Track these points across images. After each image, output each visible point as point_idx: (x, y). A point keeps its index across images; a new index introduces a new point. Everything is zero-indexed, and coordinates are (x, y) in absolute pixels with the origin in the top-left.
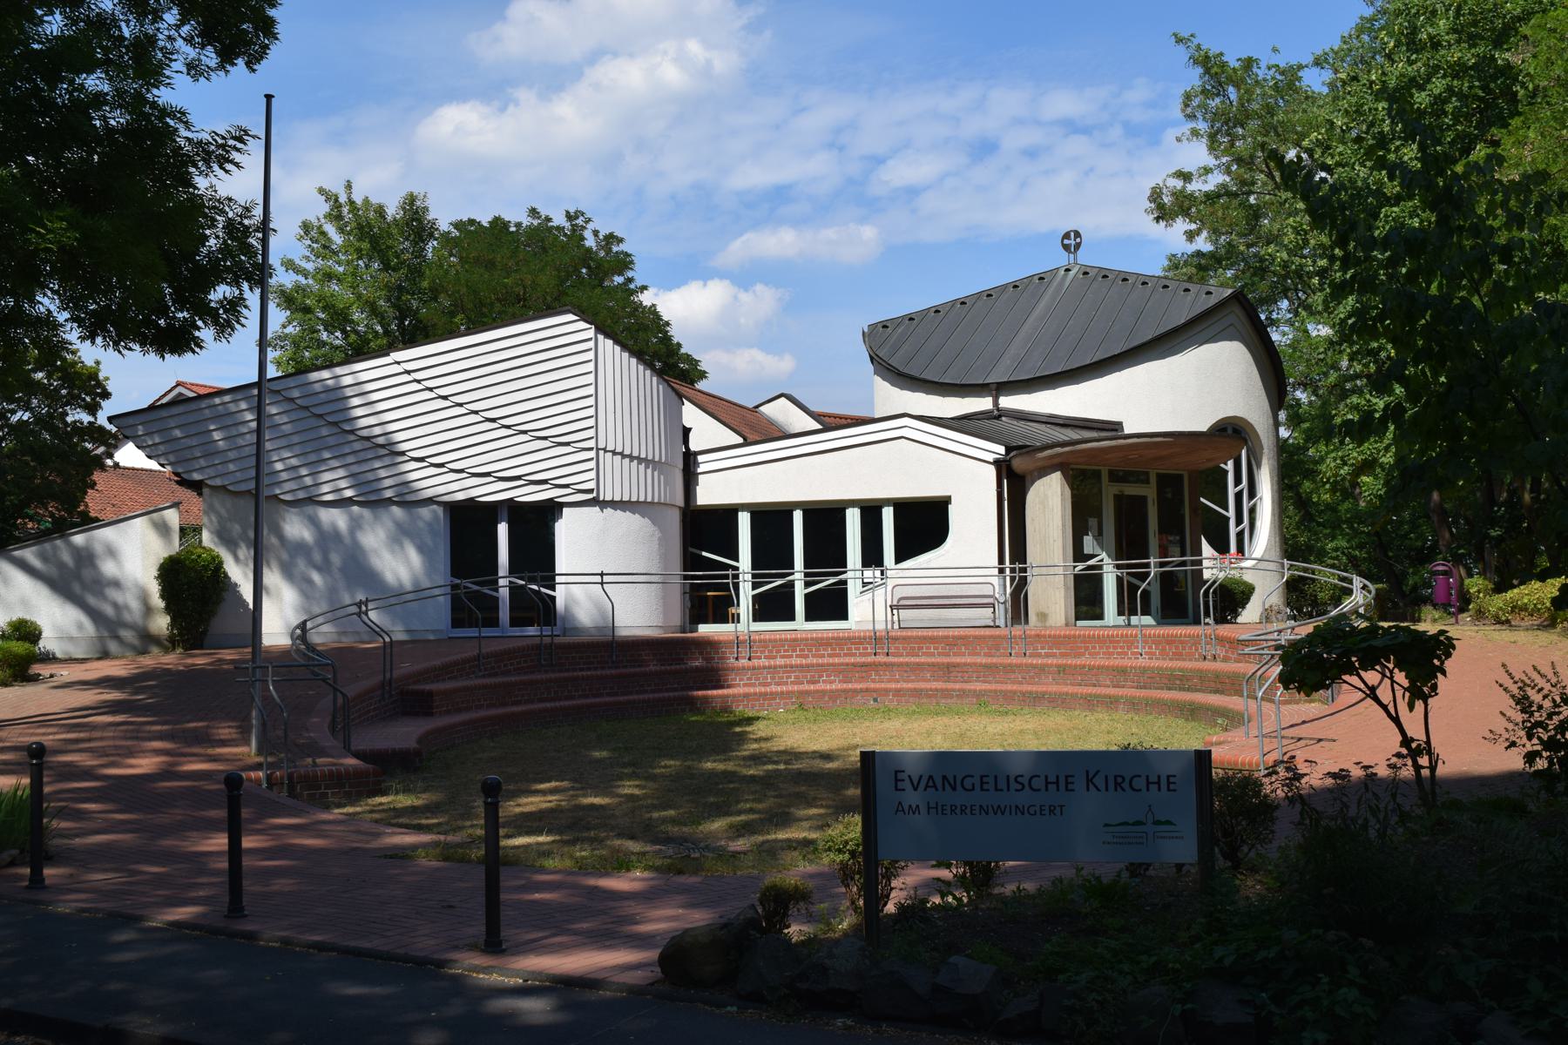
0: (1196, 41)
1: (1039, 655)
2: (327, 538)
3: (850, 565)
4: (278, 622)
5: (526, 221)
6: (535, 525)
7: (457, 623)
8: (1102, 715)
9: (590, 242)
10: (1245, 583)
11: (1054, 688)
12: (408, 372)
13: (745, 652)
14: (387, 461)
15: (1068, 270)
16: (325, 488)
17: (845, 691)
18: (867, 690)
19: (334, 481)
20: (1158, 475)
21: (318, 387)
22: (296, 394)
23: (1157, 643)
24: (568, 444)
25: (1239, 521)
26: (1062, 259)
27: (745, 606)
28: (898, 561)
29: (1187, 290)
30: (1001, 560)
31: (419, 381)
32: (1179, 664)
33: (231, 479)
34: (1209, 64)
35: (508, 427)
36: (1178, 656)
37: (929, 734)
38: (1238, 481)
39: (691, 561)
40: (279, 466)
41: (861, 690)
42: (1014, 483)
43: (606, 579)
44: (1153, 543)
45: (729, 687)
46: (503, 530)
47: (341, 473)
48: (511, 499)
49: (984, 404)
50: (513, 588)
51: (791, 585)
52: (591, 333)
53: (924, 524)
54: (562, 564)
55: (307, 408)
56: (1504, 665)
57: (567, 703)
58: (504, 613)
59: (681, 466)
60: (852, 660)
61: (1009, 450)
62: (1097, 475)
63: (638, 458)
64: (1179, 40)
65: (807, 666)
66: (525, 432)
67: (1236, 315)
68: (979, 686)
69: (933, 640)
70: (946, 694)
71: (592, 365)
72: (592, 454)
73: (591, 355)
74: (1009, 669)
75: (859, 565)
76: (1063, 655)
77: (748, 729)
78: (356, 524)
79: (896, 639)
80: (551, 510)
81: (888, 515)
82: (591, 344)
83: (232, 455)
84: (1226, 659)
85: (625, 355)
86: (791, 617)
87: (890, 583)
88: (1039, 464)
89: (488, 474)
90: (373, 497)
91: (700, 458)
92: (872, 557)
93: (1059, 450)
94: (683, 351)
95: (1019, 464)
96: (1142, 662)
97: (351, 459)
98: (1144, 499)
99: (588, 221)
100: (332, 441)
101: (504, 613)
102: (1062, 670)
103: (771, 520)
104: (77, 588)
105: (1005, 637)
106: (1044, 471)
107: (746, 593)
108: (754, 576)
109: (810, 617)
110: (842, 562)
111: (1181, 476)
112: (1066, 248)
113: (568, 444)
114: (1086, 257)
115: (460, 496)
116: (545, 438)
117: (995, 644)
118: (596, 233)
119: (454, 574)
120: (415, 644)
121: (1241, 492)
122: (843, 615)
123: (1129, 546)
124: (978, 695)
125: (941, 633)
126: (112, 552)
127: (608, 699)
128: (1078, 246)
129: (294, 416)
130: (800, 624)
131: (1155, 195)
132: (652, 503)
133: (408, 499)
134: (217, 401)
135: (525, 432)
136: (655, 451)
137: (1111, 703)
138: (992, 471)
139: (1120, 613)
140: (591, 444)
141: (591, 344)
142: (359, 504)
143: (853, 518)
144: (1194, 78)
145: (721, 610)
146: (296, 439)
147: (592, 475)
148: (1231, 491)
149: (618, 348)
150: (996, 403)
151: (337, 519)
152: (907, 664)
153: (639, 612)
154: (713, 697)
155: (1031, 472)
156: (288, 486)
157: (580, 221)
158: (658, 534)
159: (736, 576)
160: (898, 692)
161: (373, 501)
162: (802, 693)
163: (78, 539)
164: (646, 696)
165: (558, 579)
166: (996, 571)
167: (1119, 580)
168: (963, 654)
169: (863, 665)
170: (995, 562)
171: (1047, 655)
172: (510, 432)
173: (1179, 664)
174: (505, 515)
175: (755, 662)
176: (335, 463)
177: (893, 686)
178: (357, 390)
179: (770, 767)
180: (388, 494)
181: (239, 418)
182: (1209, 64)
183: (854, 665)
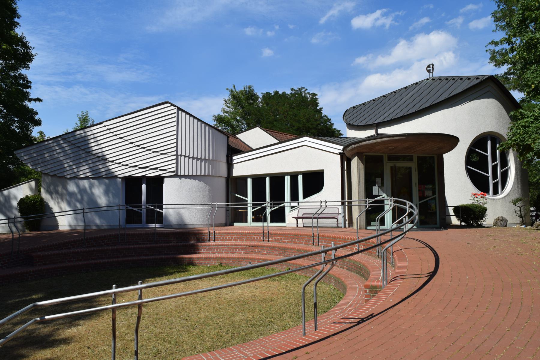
2: (82, 191)
3: (286, 200)
4: (65, 223)
6: (156, 184)
14: (102, 162)
16: (81, 173)
18: (247, 258)
19: (85, 171)
20: (418, 157)
21: (78, 136)
22: (71, 139)
24: (166, 154)
26: (427, 75)
28: (304, 198)
30: (343, 197)
35: (144, 148)
40: (66, 165)
45: (199, 253)
46: (144, 187)
47: (86, 167)
48: (145, 175)
50: (148, 210)
53: (314, 181)
54: (166, 200)
65: (231, 245)
66: (150, 150)
71: (176, 123)
72: (175, 157)
78: (91, 186)
81: (300, 178)
83: (51, 162)
89: (136, 166)
90: (97, 176)
92: (294, 197)
93: (353, 146)
95: (347, 154)
97: (90, 162)
98: (410, 168)
99: (306, 90)
103: (259, 180)
107: (250, 211)
110: (283, 199)
112: (429, 71)
113: (166, 154)
114: (437, 73)
115: (128, 174)
116: (157, 152)
122: (284, 221)
127: (144, 258)
133: (111, 177)
134: (46, 143)
135: (150, 150)
143: (287, 179)
146: (72, 155)
147: (175, 165)
150: (376, 132)
151: (85, 184)
153: (194, 218)
154: (186, 258)
156: (68, 173)
157: (303, 90)
158: (208, 188)
161: (97, 176)
162: (221, 258)
165: (164, 206)
169: (253, 246)
170: (340, 199)
172: (145, 150)
174: (145, 182)
175: (217, 243)
176: (84, 164)
178: (92, 137)
181: (53, 148)
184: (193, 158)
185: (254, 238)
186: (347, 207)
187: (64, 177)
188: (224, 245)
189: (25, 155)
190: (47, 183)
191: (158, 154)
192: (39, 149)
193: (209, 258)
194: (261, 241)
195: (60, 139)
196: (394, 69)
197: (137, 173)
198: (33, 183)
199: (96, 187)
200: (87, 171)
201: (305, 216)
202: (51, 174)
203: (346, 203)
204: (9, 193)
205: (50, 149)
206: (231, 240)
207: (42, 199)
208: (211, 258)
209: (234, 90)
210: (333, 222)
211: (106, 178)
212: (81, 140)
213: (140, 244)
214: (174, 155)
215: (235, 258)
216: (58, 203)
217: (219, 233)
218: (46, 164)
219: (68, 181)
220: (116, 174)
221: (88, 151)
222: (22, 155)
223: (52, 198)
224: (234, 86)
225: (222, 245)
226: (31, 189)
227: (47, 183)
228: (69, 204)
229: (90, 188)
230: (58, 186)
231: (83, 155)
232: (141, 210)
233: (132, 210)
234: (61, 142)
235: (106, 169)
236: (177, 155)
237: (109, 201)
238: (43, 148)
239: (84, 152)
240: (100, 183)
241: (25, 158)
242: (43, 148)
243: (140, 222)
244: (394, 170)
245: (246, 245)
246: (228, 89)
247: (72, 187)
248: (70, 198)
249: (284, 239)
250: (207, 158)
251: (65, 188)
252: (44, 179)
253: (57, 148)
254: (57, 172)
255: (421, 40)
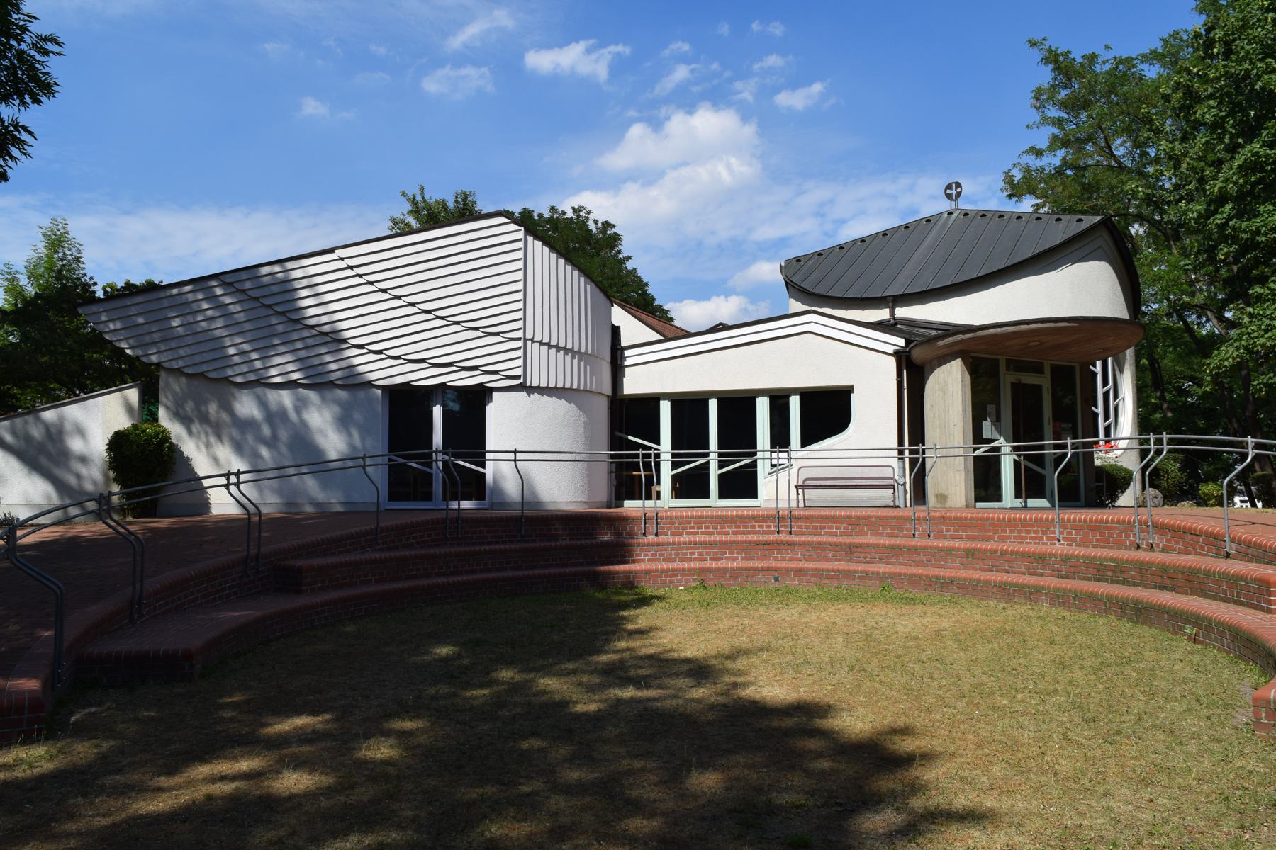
0: (1047, 44)
1: (944, 537)
2: (275, 417)
3: (760, 446)
5: (547, 215)
6: (470, 405)
7: (393, 496)
8: (1022, 609)
9: (592, 226)
10: (1121, 469)
11: (963, 574)
12: (351, 268)
13: (652, 528)
14: (332, 347)
15: (950, 213)
16: (273, 372)
17: (746, 569)
18: (768, 569)
19: (282, 366)
21: (266, 280)
22: (248, 285)
23: (1078, 529)
24: (497, 334)
25: (1107, 417)
27: (665, 485)
29: (1059, 220)
30: (901, 442)
31: (361, 276)
32: (1101, 552)
33: (188, 361)
34: (1055, 60)
35: (442, 318)
36: (1103, 543)
37: (828, 633)
38: (1105, 383)
39: (616, 442)
40: (232, 351)
41: (763, 569)
42: (913, 374)
43: (519, 456)
44: (1048, 428)
45: (634, 562)
46: (437, 411)
47: (289, 358)
49: (882, 314)
51: (706, 465)
52: (521, 235)
54: (491, 442)
55: (256, 299)
57: (470, 577)
58: (438, 488)
59: (609, 359)
60: (755, 538)
61: (908, 342)
62: (995, 363)
63: (565, 349)
64: (1033, 44)
65: (711, 543)
66: (458, 323)
67: (1104, 239)
68: (882, 568)
69: (835, 519)
70: (848, 575)
72: (520, 344)
73: (520, 254)
74: (914, 551)
75: (767, 446)
76: (969, 538)
78: (301, 405)
79: (799, 518)
80: (480, 395)
81: (795, 402)
82: (521, 244)
84: (1166, 549)
85: (554, 256)
86: (706, 495)
87: (796, 464)
88: (939, 352)
89: (423, 361)
90: (318, 380)
91: (627, 353)
92: (780, 439)
93: (960, 337)
94: (656, 303)
95: (918, 354)
96: (1059, 548)
97: (299, 345)
98: (1038, 389)
99: (589, 213)
100: (280, 328)
101: (438, 488)
102: (971, 553)
103: (689, 408)
104: (43, 461)
105: (908, 518)
106: (944, 359)
107: (666, 473)
108: (673, 456)
109: (722, 496)
111: (1073, 368)
112: (949, 196)
113: (497, 334)
114: (963, 205)
115: (399, 380)
116: (476, 329)
117: (898, 525)
118: (596, 222)
119: (392, 448)
120: (352, 513)
122: (753, 494)
123: (1024, 429)
124: (881, 577)
125: (843, 512)
126: (81, 431)
128: (959, 194)
129: (247, 306)
130: (714, 501)
131: (1009, 179)
132: (578, 390)
133: (355, 383)
134: (175, 291)
135: (458, 323)
136: (581, 342)
137: (1031, 594)
138: (892, 362)
139: (1018, 495)
140: (519, 334)
141: (521, 244)
142: (304, 386)
143: (763, 405)
144: (1045, 76)
145: (648, 490)
146: (248, 326)
147: (520, 362)
148: (1100, 391)
149: (546, 249)
150: (892, 314)
152: (810, 543)
153: (562, 487)
154: (618, 572)
155: (931, 361)
156: (238, 370)
158: (583, 418)
159: (657, 456)
160: (800, 572)
161: (319, 383)
162: (702, 570)
163: (49, 415)
164: (552, 571)
165: (488, 456)
166: (895, 453)
167: (1017, 464)
168: (865, 534)
170: (895, 444)
171: (953, 538)
172: (444, 323)
173: (1101, 552)
175: (661, 538)
176: (283, 349)
177: (795, 565)
178: (305, 282)
179: (628, 693)
180: (334, 376)
182: (1055, 60)
183: (756, 543)
184: (558, 348)
185: (753, 527)
186: (907, 460)
187: (226, 379)
188: (695, 543)
189: (113, 320)
190: (174, 394)
191: (478, 334)
192: (154, 306)
193: (673, 570)
194: (773, 532)
195: (214, 283)
196: (624, 181)
197: (425, 377)
198: (133, 395)
199: (313, 409)
200: (290, 368)
201: (808, 483)
202: (190, 371)
203: (907, 452)
204: (61, 419)
205: (185, 308)
206: (696, 533)
207: (164, 437)
208: (678, 570)
209: (419, 198)
210: (884, 496)
211: (342, 387)
212: (275, 289)
213: (490, 543)
214: (519, 339)
215: (738, 569)
216: (208, 446)
217: (667, 518)
218: (173, 344)
219: (235, 391)
220: (372, 376)
221: (294, 317)
222: (104, 318)
223: (190, 433)
224: (422, 188)
225: (690, 543)
226: (129, 409)
227: (174, 394)
228: (239, 448)
229: (298, 410)
230: (206, 402)
231: (280, 328)
232: (430, 465)
233: (404, 464)
234: (219, 291)
235: (344, 364)
236: (525, 340)
237: (352, 446)
238: (166, 303)
239: (283, 319)
240: (323, 399)
241: (112, 326)
242: (166, 303)
243: (428, 496)
244: (1016, 387)
245: (750, 542)
246: (404, 194)
247: (246, 406)
248: (241, 434)
249: (831, 527)
250: (583, 350)
251: (227, 407)
252: (167, 384)
253: (205, 306)
254: (204, 368)
255: (678, 123)
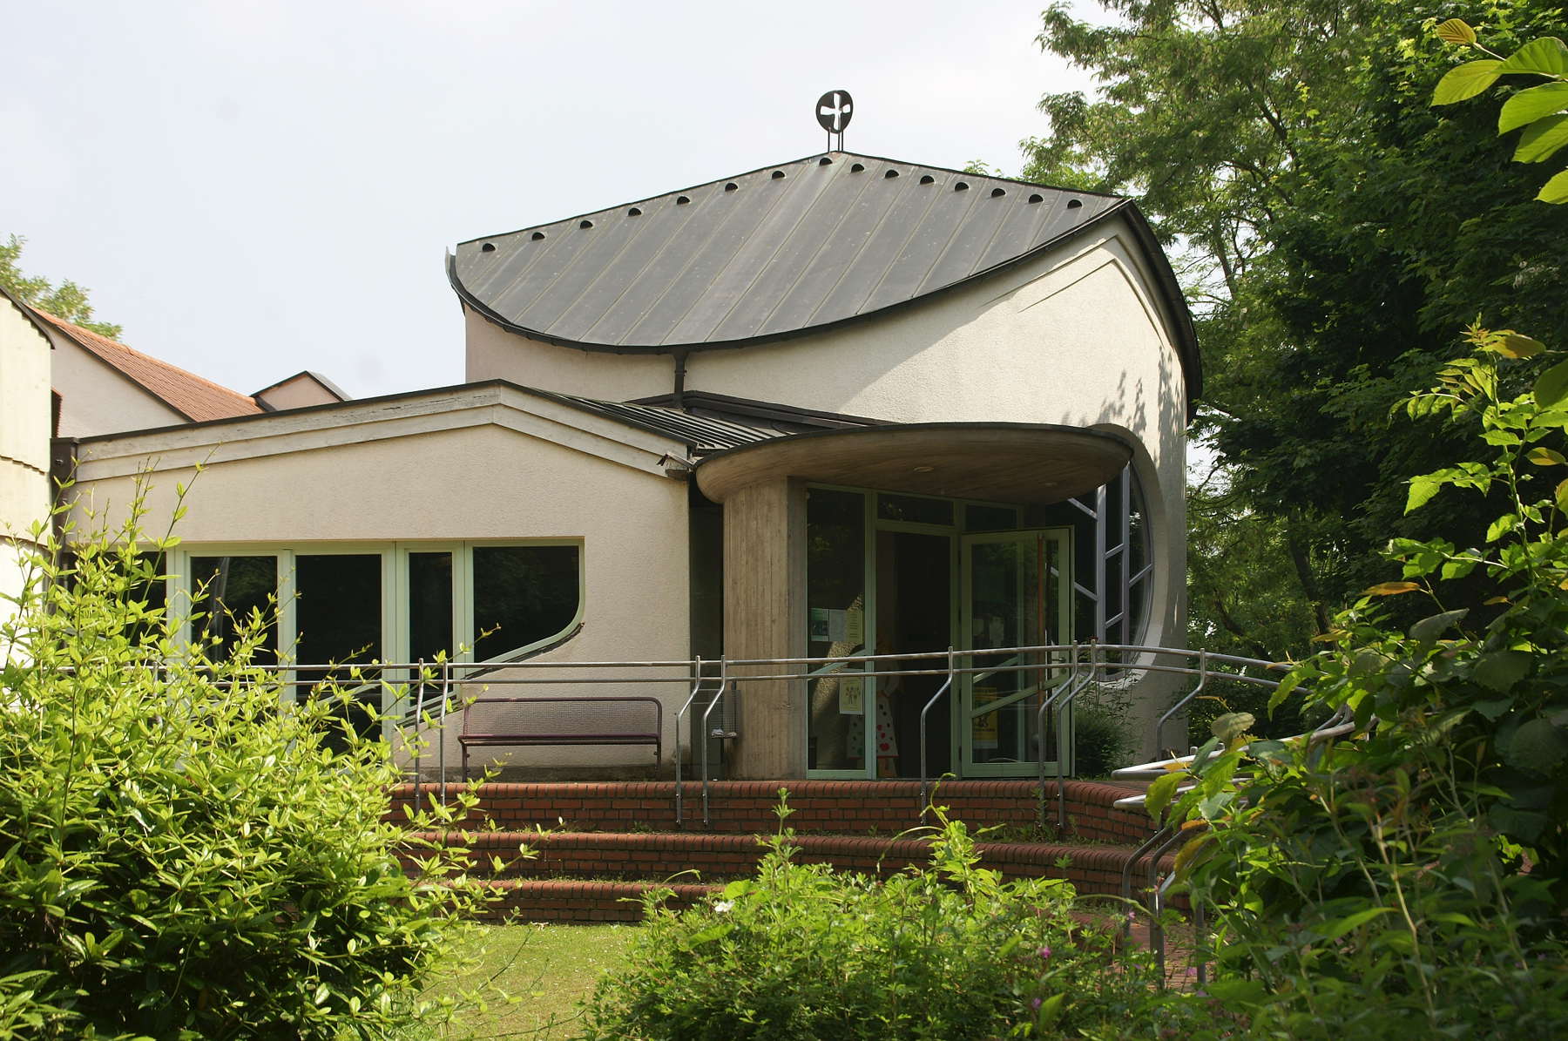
15: (825, 162)
26: (817, 141)
56: (1124, 375)
77: (342, 901)
112: (826, 122)
114: (858, 139)
121: (1118, 557)
128: (846, 119)
